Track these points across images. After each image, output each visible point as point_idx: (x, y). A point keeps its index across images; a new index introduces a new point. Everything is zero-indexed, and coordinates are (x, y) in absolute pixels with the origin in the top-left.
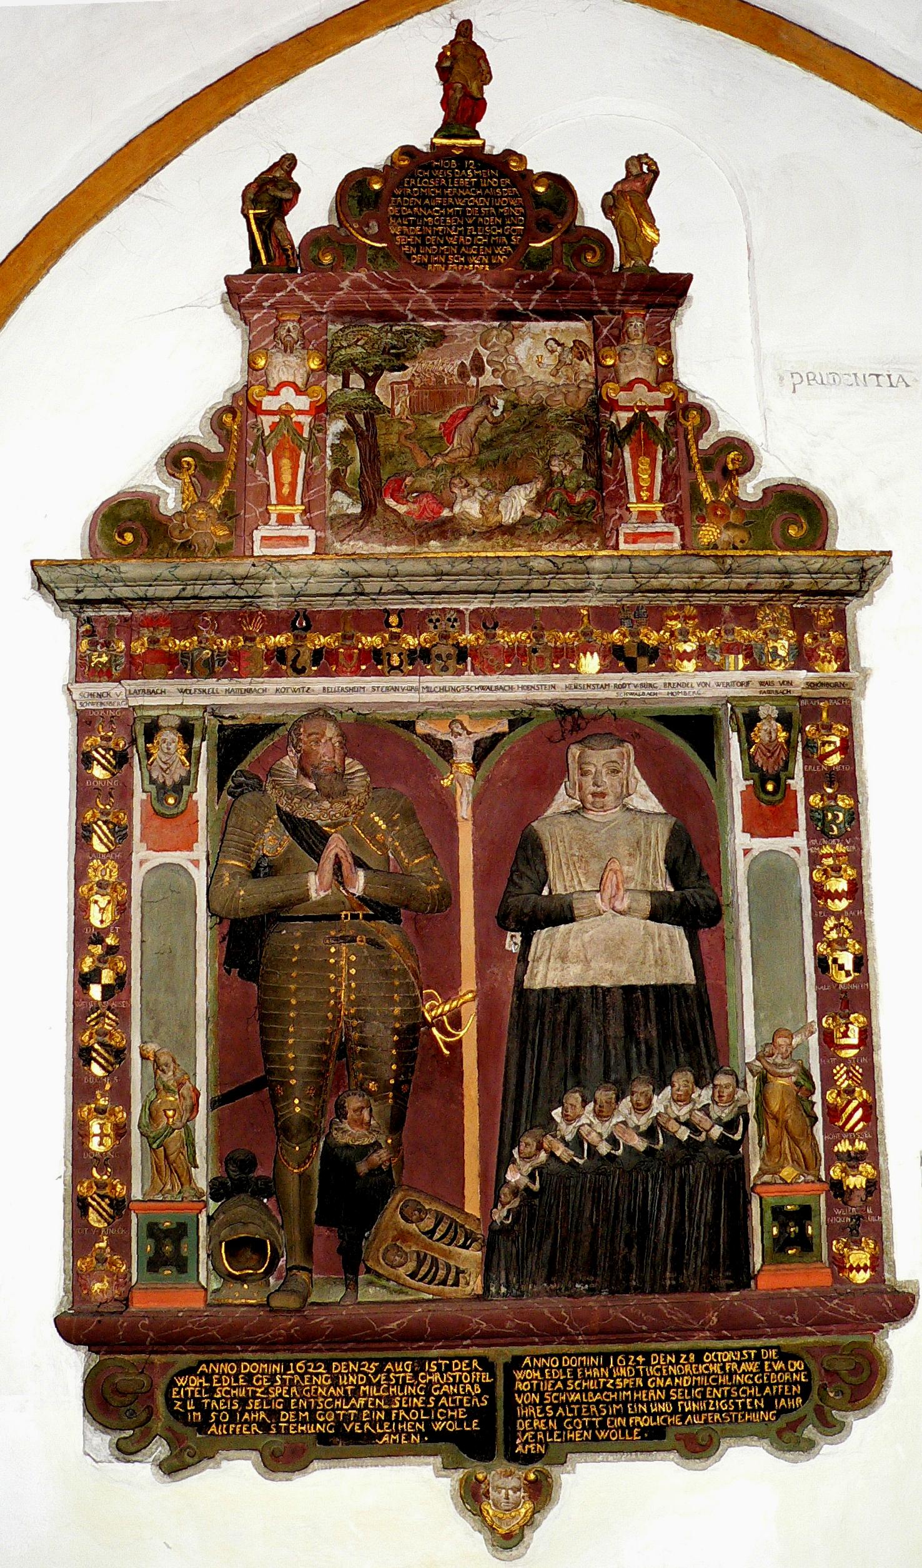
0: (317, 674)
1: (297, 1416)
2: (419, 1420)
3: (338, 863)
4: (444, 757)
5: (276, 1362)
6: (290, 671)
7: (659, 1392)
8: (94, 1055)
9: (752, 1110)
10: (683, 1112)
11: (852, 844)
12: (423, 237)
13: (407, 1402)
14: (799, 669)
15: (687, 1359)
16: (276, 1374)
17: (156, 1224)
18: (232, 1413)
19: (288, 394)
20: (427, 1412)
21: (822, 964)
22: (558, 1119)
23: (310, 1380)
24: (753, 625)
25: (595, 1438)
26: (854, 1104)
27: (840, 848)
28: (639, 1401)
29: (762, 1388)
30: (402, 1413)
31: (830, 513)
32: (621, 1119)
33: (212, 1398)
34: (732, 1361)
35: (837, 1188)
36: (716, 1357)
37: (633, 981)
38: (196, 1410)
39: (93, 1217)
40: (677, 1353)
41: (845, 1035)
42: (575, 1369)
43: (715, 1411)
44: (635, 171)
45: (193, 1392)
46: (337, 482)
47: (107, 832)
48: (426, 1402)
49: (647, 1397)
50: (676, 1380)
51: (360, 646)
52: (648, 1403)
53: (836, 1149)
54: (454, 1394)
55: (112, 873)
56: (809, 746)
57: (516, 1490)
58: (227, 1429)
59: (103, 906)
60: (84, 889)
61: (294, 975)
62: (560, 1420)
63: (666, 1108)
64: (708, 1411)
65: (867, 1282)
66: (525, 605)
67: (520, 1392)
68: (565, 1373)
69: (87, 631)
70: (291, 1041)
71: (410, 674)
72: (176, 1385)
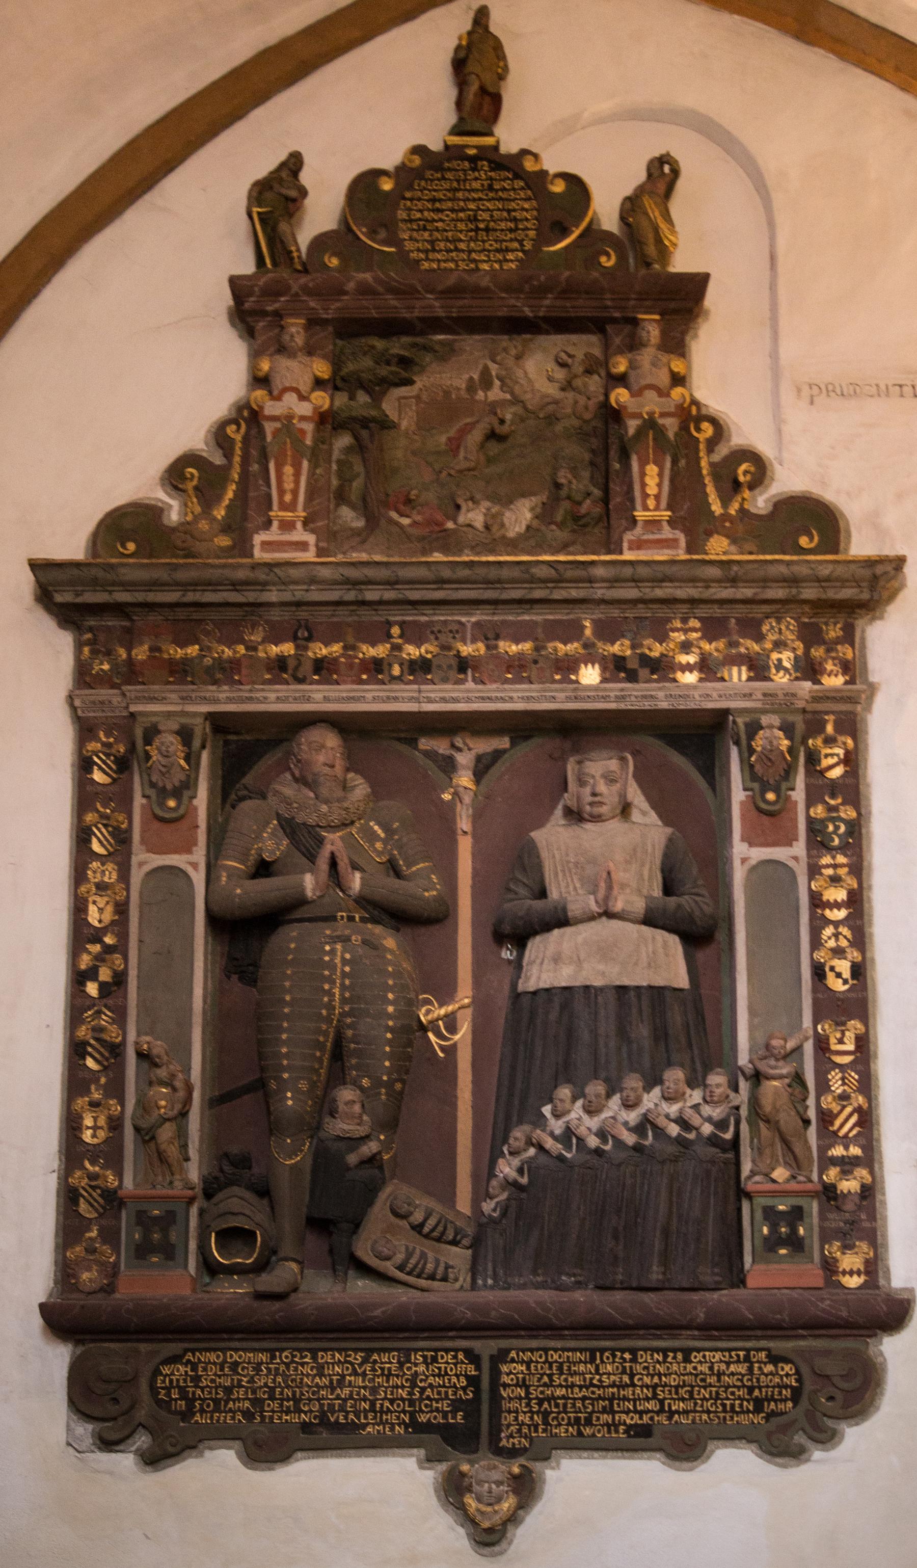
0: (318, 682)
1: (281, 1405)
2: (404, 1412)
3: (333, 863)
4: (445, 772)
5: (262, 1350)
6: (290, 679)
7: (645, 1390)
8: (90, 1049)
9: (744, 1112)
10: (673, 1109)
11: (853, 855)
12: (432, 242)
13: (392, 1394)
14: (805, 680)
15: (674, 1358)
16: (262, 1363)
17: (145, 1212)
18: (216, 1402)
19: (290, 399)
20: (412, 1403)
21: (819, 972)
22: (548, 1115)
23: (296, 1369)
24: (759, 638)
25: (580, 1434)
26: (849, 1109)
27: (841, 859)
28: (625, 1399)
29: (751, 1390)
30: (387, 1404)
31: (842, 525)
32: (611, 1114)
33: (197, 1386)
34: (721, 1361)
35: (829, 1193)
36: (704, 1357)
37: (626, 982)
38: (180, 1399)
39: (83, 1207)
40: (665, 1351)
41: (841, 1041)
42: (561, 1364)
43: (703, 1412)
44: (656, 173)
45: (178, 1380)
46: (341, 497)
48: (411, 1393)
49: (633, 1394)
50: (664, 1379)
51: (361, 655)
52: (635, 1400)
53: (830, 1153)
54: (440, 1386)
55: (110, 874)
56: (812, 759)
57: (499, 1483)
58: (212, 1418)
59: (101, 906)
60: (83, 889)
61: (289, 972)
62: (546, 1414)
63: (656, 1105)
64: (695, 1411)
65: (859, 1288)
66: (527, 618)
67: (505, 1386)
68: (551, 1368)
69: (89, 639)
70: (284, 1036)
71: (410, 682)
72: (161, 1374)
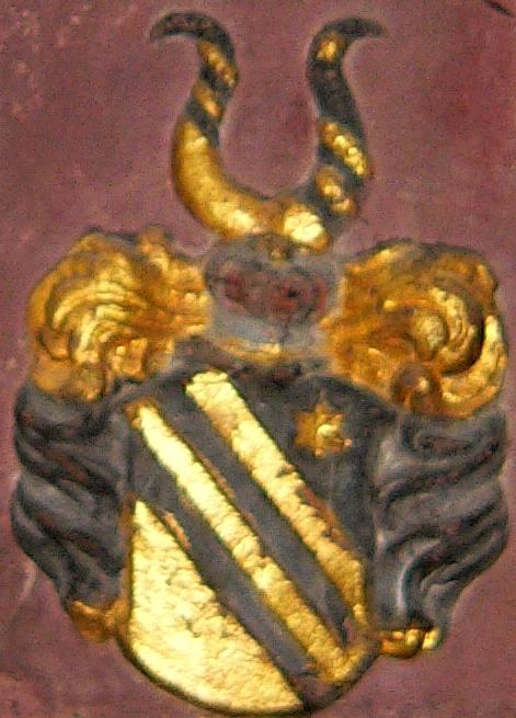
47: (283, 489)
